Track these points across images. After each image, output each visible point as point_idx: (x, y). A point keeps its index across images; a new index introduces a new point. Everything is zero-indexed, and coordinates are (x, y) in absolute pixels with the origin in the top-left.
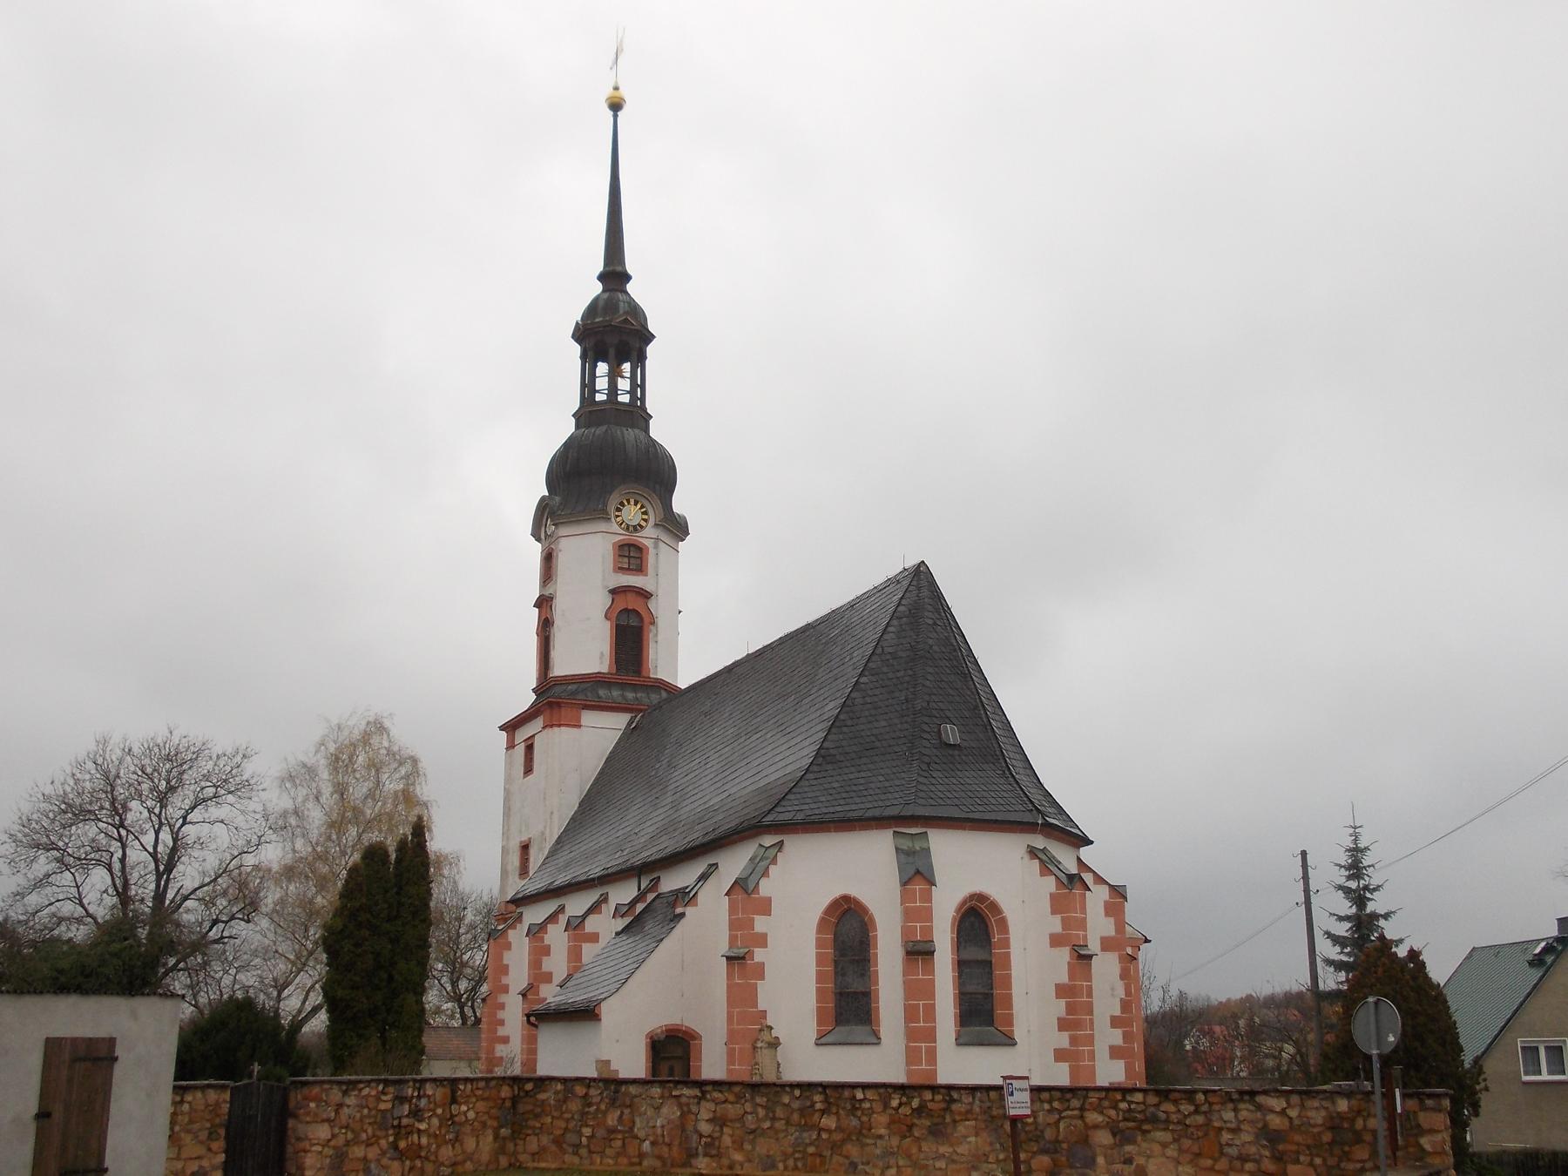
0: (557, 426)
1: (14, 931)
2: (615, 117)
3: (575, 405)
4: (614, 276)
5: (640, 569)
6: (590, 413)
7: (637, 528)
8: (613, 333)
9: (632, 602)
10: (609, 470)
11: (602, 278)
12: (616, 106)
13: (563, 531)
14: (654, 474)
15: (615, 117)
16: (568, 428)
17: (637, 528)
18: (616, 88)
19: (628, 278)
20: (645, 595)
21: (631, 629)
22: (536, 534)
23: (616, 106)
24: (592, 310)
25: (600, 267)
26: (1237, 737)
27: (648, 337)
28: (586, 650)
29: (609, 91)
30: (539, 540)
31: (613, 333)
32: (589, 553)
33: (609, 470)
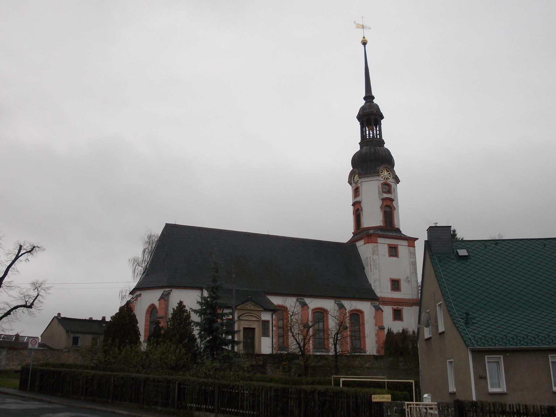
0: (353, 146)
1: (189, 316)
2: (365, 47)
3: (359, 140)
4: (369, 97)
5: (389, 192)
6: (364, 141)
7: (387, 179)
8: (370, 117)
9: (388, 203)
10: (372, 160)
11: (365, 98)
12: (364, 43)
13: (363, 180)
14: (387, 161)
15: (365, 47)
16: (358, 148)
17: (387, 179)
18: (364, 38)
19: (373, 98)
20: (392, 200)
21: (389, 209)
22: (350, 182)
23: (364, 43)
24: (363, 109)
25: (364, 95)
26: (466, 170)
27: (382, 117)
28: (373, 218)
29: (362, 39)
30: (351, 184)
31: (370, 117)
32: (371, 188)
33: (372, 160)
